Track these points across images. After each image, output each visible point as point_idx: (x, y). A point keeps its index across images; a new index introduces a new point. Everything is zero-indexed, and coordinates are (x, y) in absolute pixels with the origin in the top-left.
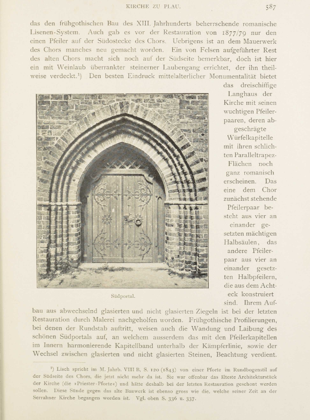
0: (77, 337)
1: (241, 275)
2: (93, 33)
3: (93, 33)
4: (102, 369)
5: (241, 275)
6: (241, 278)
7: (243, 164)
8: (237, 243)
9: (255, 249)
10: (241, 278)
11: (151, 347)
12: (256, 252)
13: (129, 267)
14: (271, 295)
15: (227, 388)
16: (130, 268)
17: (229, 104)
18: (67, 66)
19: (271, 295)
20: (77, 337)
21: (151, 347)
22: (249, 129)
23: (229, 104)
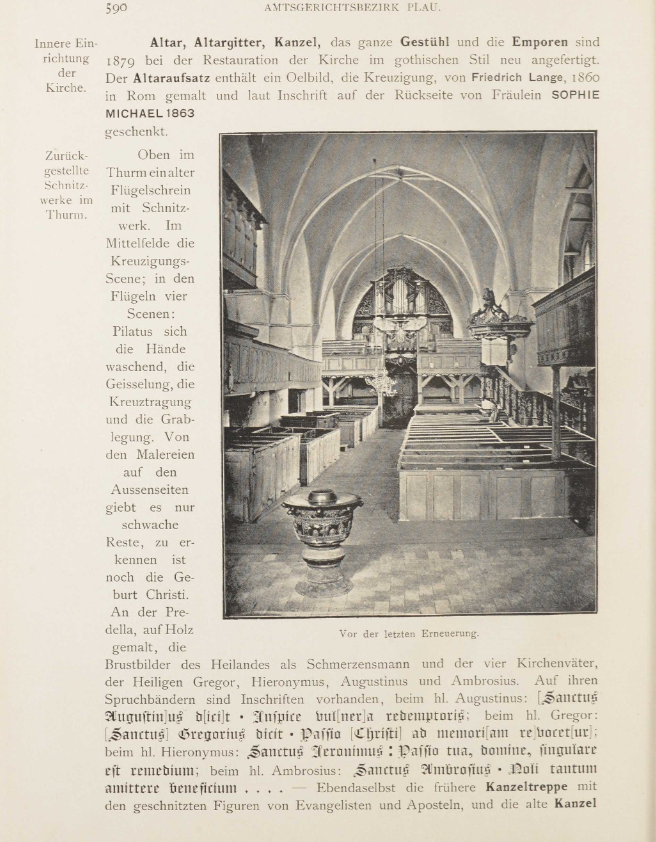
0: (117, 578)
1: (216, 662)
2: (121, 614)
3: (121, 614)
4: (492, 43)
5: (216, 662)
6: (217, 667)
7: (379, 787)
8: (382, 789)
9: (117, 329)
10: (217, 667)
11: (596, 43)
12: (119, 333)
13: (394, 294)
14: (132, 596)
15: (456, 797)
16: (392, 296)
17: (527, 665)
18: (180, 188)
19: (132, 596)
20: (117, 578)
21: (596, 43)
22: (138, 526)
23: (527, 665)
